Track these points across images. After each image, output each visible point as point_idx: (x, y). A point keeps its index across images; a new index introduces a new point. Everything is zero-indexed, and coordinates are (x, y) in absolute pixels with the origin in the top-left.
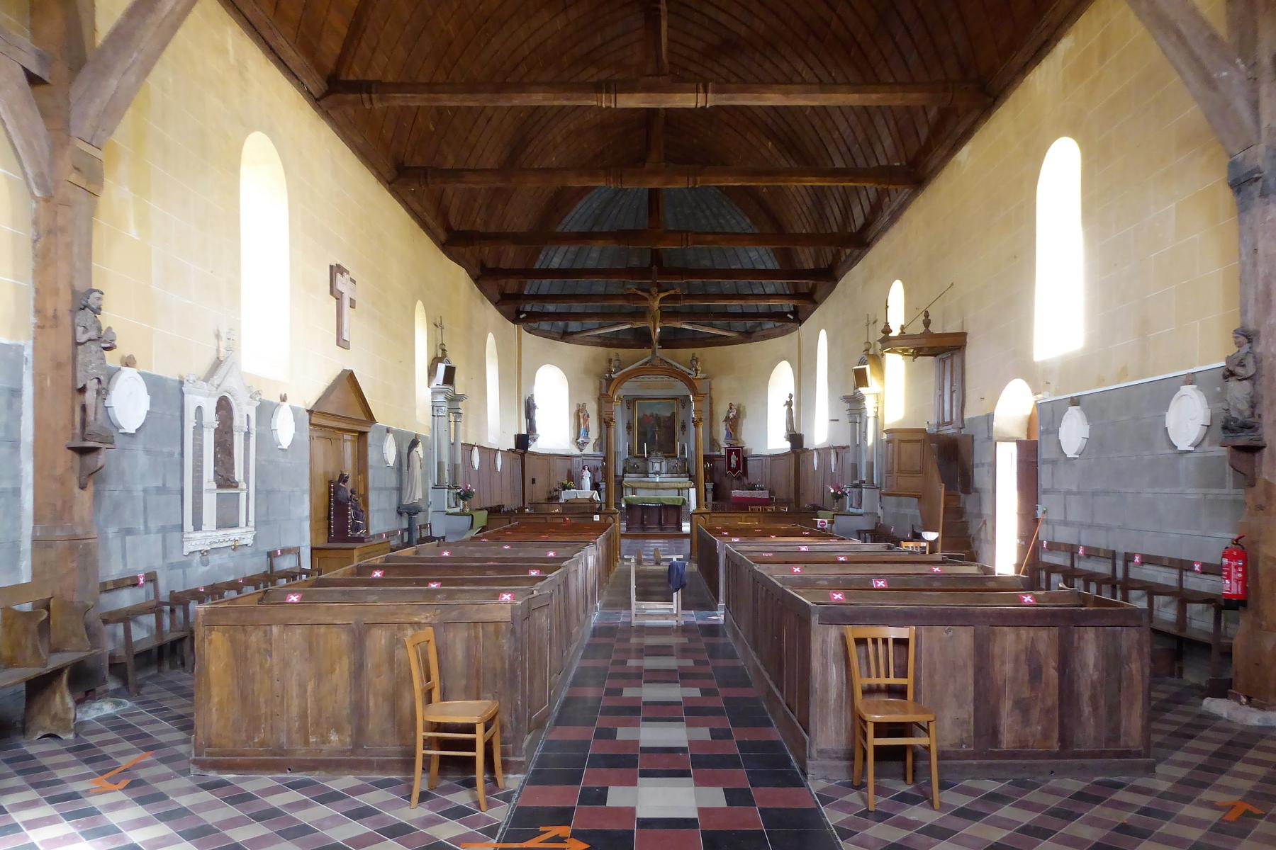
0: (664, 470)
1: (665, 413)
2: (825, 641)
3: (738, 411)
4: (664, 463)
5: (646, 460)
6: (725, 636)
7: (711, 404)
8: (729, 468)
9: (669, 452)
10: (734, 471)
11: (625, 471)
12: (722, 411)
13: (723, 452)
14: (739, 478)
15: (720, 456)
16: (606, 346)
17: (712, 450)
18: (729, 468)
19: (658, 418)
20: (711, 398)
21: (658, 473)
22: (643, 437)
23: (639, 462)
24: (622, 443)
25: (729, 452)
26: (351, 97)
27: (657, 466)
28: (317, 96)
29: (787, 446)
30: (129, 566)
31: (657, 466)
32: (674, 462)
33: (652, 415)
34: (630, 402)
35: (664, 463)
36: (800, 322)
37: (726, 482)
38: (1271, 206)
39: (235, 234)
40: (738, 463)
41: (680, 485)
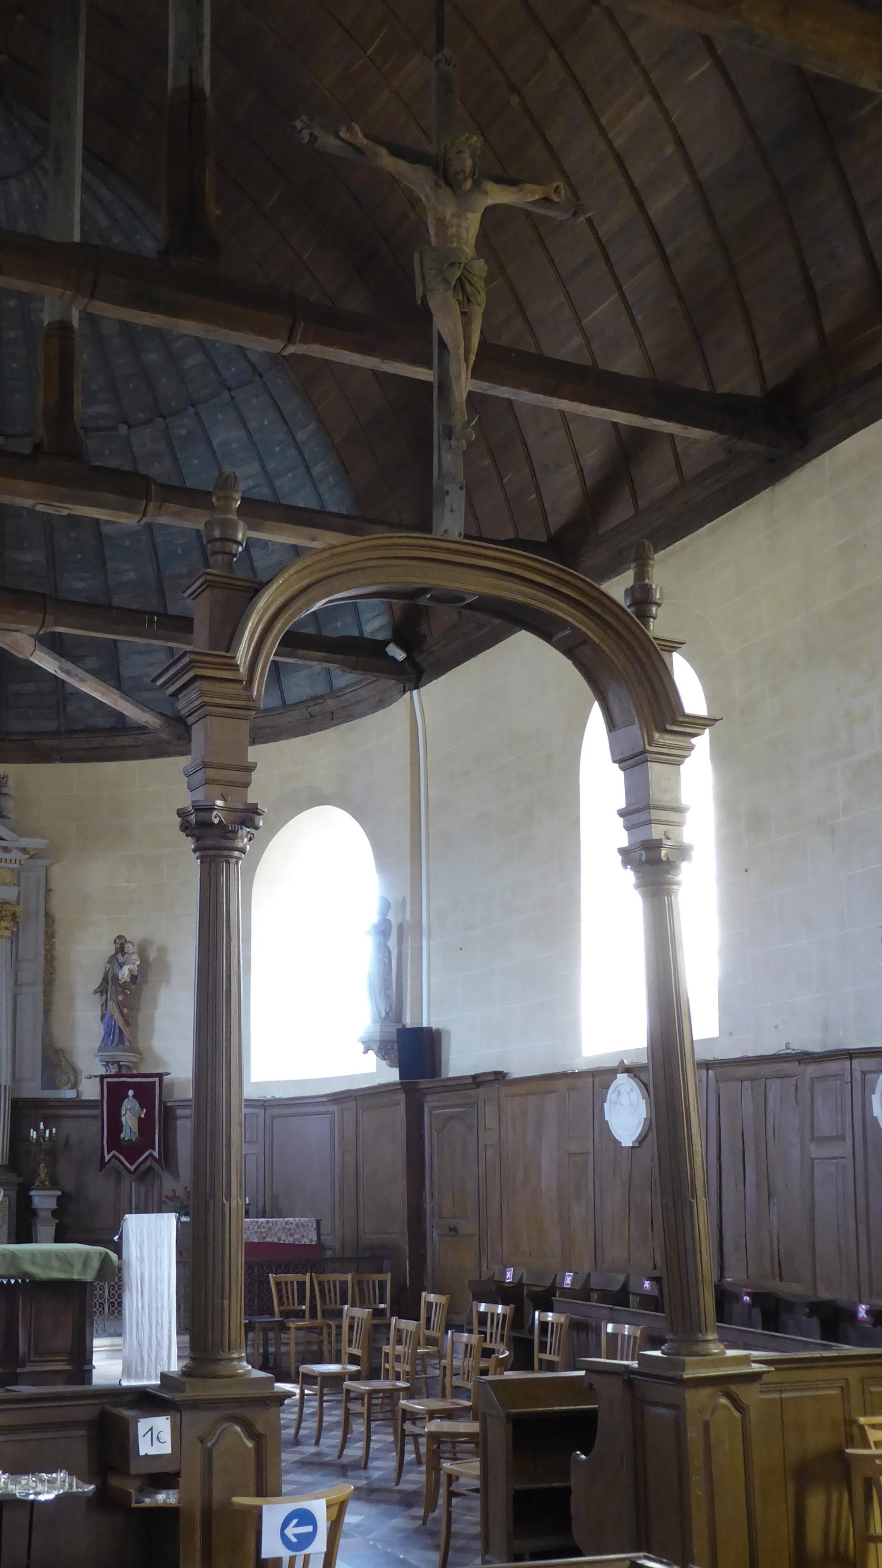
2: (525, 1287)
3: (145, 964)
7: (50, 936)
8: (115, 1141)
10: (132, 1151)
12: (85, 956)
13: (90, 1090)
14: (144, 1176)
15: (79, 1103)
17: (50, 1082)
18: (115, 1141)
20: (49, 916)
25: (115, 1092)
28: (867, 1076)
29: (369, 1069)
36: (415, 675)
37: (98, 1186)
38: (425, 1506)
39: (190, 741)
40: (145, 1125)
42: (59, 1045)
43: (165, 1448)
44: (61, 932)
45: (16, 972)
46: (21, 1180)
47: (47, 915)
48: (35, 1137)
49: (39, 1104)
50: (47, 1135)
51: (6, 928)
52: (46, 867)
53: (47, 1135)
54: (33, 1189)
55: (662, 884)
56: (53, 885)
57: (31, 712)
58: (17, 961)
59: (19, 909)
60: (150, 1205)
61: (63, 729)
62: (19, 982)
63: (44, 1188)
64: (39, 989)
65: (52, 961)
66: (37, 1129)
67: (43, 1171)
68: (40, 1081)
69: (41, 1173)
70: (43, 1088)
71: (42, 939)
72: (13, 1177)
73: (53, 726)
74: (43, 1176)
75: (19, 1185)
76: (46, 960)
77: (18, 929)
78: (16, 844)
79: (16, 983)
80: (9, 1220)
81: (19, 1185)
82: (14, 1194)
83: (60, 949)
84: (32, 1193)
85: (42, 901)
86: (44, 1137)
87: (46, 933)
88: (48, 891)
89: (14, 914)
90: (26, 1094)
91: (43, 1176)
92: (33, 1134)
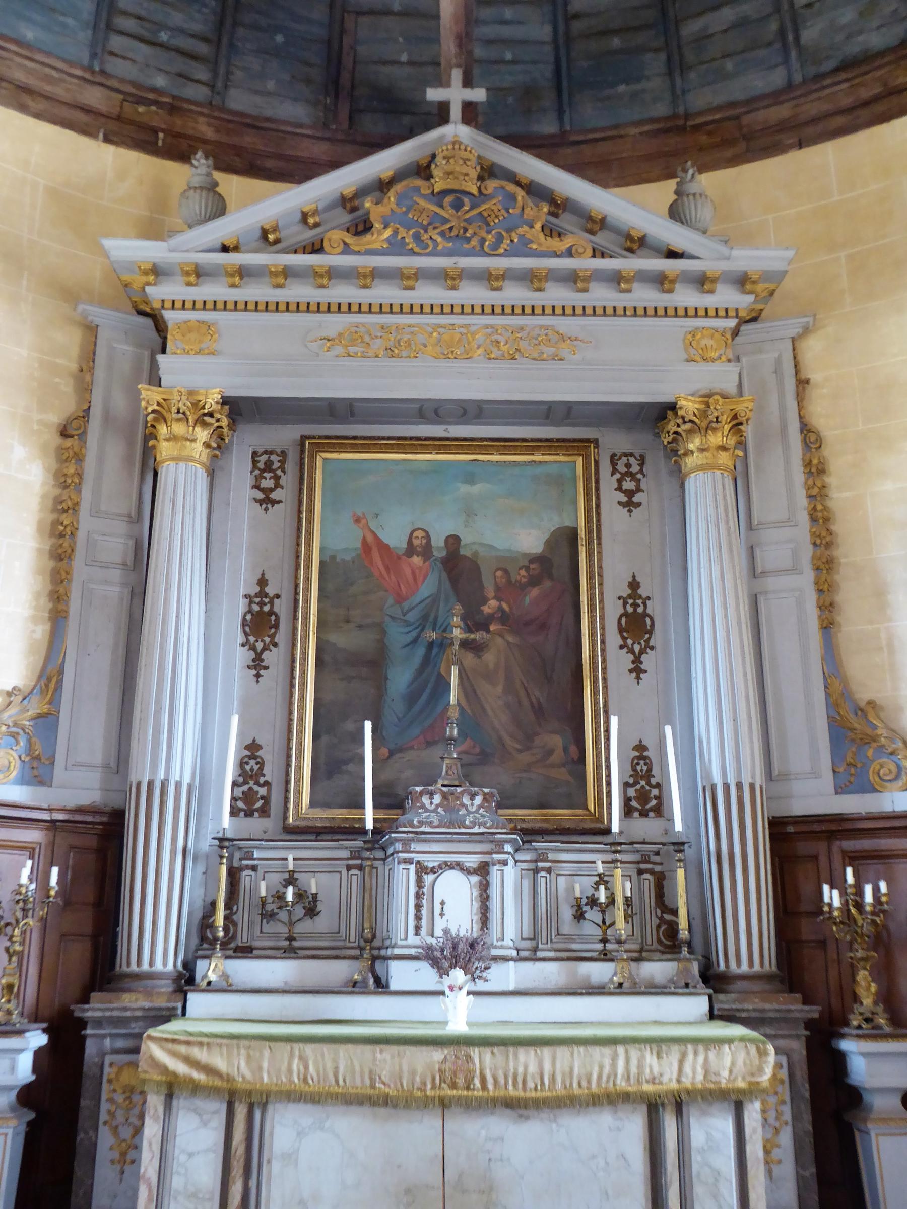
0: (510, 925)
1: (514, 533)
4: (508, 879)
5: (372, 848)
6: (347, 250)
9: (547, 801)
11: (203, 938)
16: (144, 139)
17: (852, 775)
19: (457, 565)
20: (811, 437)
21: (460, 955)
22: (353, 679)
23: (325, 873)
24: (200, 721)
26: (637, 1046)
27: (455, 897)
30: (289, 1048)
31: (455, 897)
32: (577, 869)
33: (418, 546)
34: (283, 441)
35: (508, 879)
41: (665, 1072)
42: (863, 696)
43: (283, 40)
44: (839, 464)
45: (751, 550)
46: (814, 1012)
47: (806, 429)
48: (837, 903)
49: (834, 827)
50: (869, 898)
51: (723, 448)
52: (793, 339)
53: (869, 898)
54: (843, 1036)
55: (185, 1081)
56: (815, 375)
57: (729, 65)
58: (750, 527)
59: (743, 407)
60: (867, 883)
61: (798, 78)
62: (759, 570)
63: (877, 1035)
64: (806, 579)
65: (827, 520)
66: (837, 882)
67: (867, 988)
68: (828, 776)
69: (861, 992)
70: (839, 790)
71: (799, 476)
72: (796, 1007)
73: (776, 78)
74: (868, 1002)
75: (809, 1024)
76: (814, 520)
77: (745, 451)
78: (723, 266)
79: (754, 573)
80: (796, 1118)
81: (809, 1024)
82: (798, 1047)
83: (839, 497)
84: (846, 1045)
85: (792, 404)
86: (859, 906)
87: (808, 464)
88: (802, 383)
89: (735, 417)
90: (799, 808)
91: (868, 1002)
92: (832, 897)
